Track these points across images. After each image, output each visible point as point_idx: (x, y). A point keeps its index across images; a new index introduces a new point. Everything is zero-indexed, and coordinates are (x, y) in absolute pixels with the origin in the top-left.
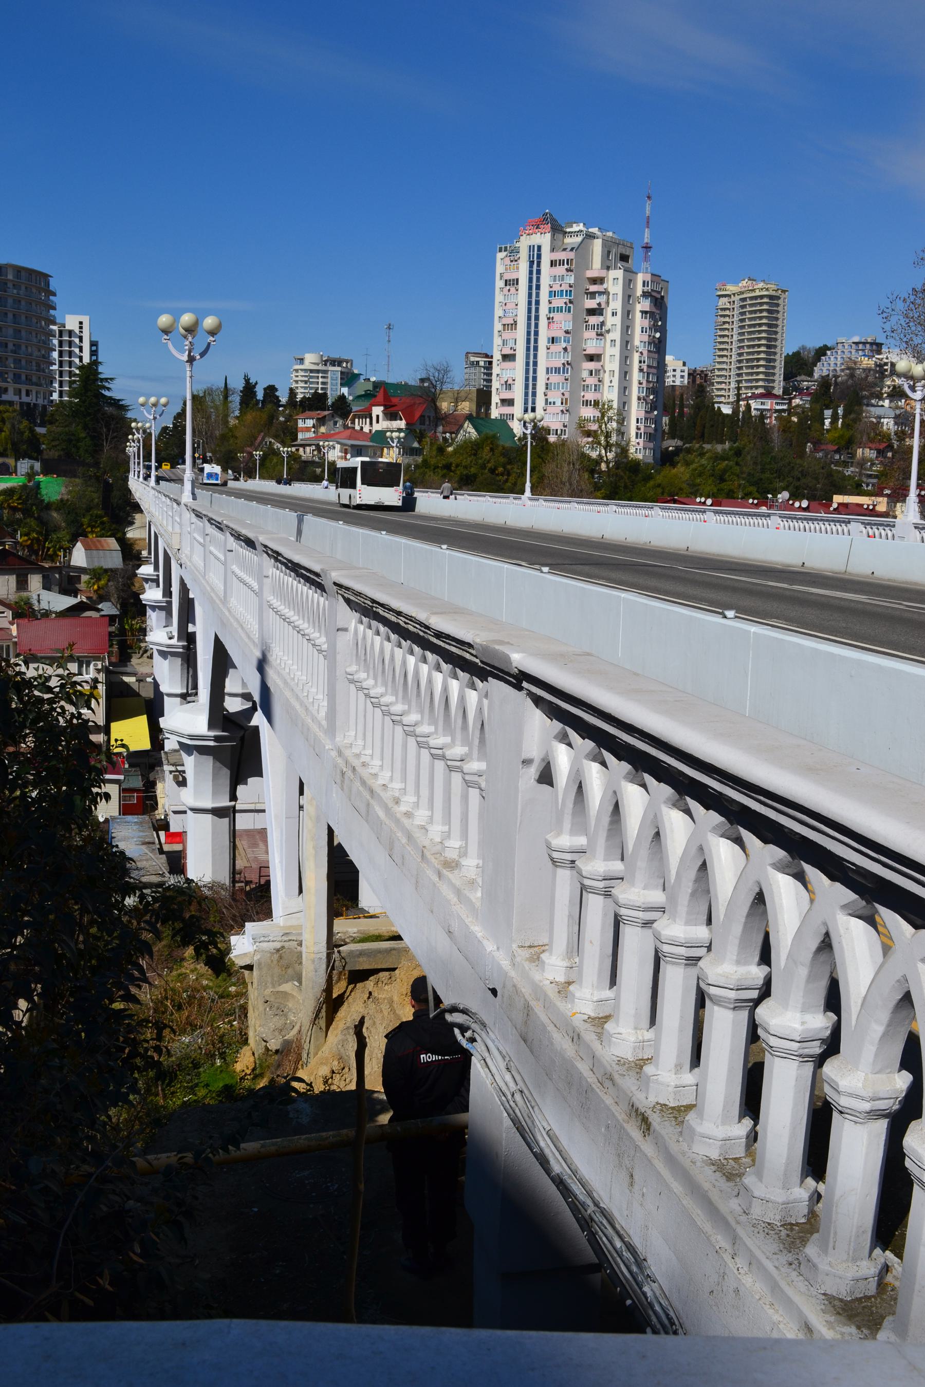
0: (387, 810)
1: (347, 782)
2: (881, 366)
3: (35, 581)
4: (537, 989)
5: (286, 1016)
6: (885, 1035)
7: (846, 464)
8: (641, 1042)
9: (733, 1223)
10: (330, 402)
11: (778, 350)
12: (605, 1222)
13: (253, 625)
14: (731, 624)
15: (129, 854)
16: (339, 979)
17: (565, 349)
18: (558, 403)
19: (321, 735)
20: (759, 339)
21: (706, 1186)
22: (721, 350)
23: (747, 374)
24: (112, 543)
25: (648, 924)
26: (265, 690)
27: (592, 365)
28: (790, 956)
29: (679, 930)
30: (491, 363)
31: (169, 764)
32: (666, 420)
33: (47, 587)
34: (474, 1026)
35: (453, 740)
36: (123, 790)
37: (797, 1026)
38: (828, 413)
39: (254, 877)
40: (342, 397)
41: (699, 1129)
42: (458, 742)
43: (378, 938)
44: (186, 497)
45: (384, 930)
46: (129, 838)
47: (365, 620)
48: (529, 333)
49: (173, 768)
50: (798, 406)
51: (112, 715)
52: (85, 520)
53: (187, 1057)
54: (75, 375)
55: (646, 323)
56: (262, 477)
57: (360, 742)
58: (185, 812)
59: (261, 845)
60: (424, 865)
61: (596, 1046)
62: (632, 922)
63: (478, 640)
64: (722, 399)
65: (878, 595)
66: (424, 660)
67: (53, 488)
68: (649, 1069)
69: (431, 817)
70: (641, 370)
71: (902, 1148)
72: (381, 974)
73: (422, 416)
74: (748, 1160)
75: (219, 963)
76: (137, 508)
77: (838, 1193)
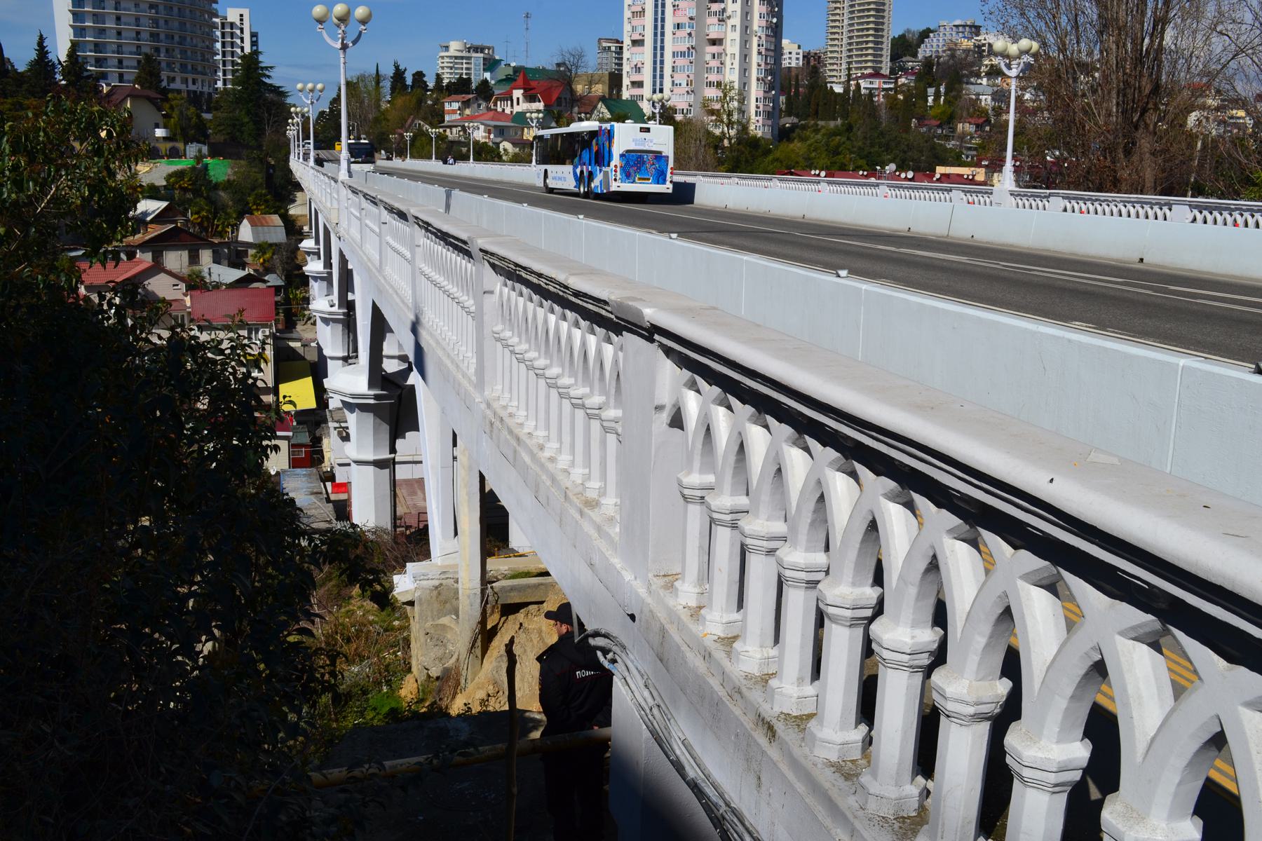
0: (533, 456)
1: (495, 431)
2: (979, 47)
3: (206, 256)
4: (671, 613)
5: (445, 646)
6: (988, 645)
7: (947, 138)
8: (766, 659)
9: (850, 816)
10: (474, 86)
11: (885, 33)
12: (735, 820)
13: (407, 292)
14: (845, 282)
15: (298, 504)
16: (493, 612)
17: (690, 34)
18: (684, 84)
19: (471, 389)
20: (868, 23)
21: (827, 785)
22: (833, 34)
23: (857, 56)
24: (276, 219)
25: (771, 552)
26: (419, 350)
27: (714, 49)
28: (901, 577)
29: (800, 556)
30: (621, 48)
31: (334, 421)
32: (782, 99)
33: (217, 261)
34: (614, 648)
35: (592, 391)
36: (293, 446)
37: (908, 640)
38: (931, 91)
39: (413, 522)
40: (485, 82)
41: (819, 735)
42: (596, 392)
43: (527, 575)
44: (343, 175)
45: (533, 567)
46: (299, 488)
47: (509, 283)
48: (656, 20)
49: (337, 425)
50: (903, 84)
51: (280, 377)
52: (250, 199)
53: (356, 685)
54: (238, 64)
55: (764, 9)
56: (412, 157)
57: (507, 395)
58: (349, 465)
59: (419, 492)
60: (566, 504)
61: (726, 663)
62: (757, 550)
63: (613, 298)
64: (834, 79)
65: (977, 256)
66: (564, 318)
67: (220, 170)
68: (773, 683)
69: (573, 461)
70: (760, 53)
71: (1003, 746)
72: (531, 607)
73: (559, 99)
74: (864, 762)
75: (383, 599)
76: (298, 187)
77: (945, 789)
